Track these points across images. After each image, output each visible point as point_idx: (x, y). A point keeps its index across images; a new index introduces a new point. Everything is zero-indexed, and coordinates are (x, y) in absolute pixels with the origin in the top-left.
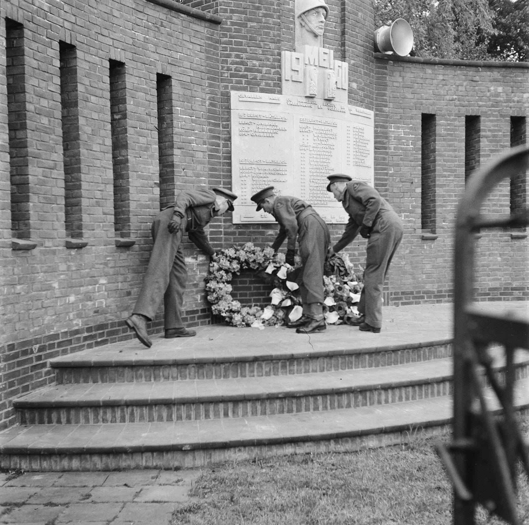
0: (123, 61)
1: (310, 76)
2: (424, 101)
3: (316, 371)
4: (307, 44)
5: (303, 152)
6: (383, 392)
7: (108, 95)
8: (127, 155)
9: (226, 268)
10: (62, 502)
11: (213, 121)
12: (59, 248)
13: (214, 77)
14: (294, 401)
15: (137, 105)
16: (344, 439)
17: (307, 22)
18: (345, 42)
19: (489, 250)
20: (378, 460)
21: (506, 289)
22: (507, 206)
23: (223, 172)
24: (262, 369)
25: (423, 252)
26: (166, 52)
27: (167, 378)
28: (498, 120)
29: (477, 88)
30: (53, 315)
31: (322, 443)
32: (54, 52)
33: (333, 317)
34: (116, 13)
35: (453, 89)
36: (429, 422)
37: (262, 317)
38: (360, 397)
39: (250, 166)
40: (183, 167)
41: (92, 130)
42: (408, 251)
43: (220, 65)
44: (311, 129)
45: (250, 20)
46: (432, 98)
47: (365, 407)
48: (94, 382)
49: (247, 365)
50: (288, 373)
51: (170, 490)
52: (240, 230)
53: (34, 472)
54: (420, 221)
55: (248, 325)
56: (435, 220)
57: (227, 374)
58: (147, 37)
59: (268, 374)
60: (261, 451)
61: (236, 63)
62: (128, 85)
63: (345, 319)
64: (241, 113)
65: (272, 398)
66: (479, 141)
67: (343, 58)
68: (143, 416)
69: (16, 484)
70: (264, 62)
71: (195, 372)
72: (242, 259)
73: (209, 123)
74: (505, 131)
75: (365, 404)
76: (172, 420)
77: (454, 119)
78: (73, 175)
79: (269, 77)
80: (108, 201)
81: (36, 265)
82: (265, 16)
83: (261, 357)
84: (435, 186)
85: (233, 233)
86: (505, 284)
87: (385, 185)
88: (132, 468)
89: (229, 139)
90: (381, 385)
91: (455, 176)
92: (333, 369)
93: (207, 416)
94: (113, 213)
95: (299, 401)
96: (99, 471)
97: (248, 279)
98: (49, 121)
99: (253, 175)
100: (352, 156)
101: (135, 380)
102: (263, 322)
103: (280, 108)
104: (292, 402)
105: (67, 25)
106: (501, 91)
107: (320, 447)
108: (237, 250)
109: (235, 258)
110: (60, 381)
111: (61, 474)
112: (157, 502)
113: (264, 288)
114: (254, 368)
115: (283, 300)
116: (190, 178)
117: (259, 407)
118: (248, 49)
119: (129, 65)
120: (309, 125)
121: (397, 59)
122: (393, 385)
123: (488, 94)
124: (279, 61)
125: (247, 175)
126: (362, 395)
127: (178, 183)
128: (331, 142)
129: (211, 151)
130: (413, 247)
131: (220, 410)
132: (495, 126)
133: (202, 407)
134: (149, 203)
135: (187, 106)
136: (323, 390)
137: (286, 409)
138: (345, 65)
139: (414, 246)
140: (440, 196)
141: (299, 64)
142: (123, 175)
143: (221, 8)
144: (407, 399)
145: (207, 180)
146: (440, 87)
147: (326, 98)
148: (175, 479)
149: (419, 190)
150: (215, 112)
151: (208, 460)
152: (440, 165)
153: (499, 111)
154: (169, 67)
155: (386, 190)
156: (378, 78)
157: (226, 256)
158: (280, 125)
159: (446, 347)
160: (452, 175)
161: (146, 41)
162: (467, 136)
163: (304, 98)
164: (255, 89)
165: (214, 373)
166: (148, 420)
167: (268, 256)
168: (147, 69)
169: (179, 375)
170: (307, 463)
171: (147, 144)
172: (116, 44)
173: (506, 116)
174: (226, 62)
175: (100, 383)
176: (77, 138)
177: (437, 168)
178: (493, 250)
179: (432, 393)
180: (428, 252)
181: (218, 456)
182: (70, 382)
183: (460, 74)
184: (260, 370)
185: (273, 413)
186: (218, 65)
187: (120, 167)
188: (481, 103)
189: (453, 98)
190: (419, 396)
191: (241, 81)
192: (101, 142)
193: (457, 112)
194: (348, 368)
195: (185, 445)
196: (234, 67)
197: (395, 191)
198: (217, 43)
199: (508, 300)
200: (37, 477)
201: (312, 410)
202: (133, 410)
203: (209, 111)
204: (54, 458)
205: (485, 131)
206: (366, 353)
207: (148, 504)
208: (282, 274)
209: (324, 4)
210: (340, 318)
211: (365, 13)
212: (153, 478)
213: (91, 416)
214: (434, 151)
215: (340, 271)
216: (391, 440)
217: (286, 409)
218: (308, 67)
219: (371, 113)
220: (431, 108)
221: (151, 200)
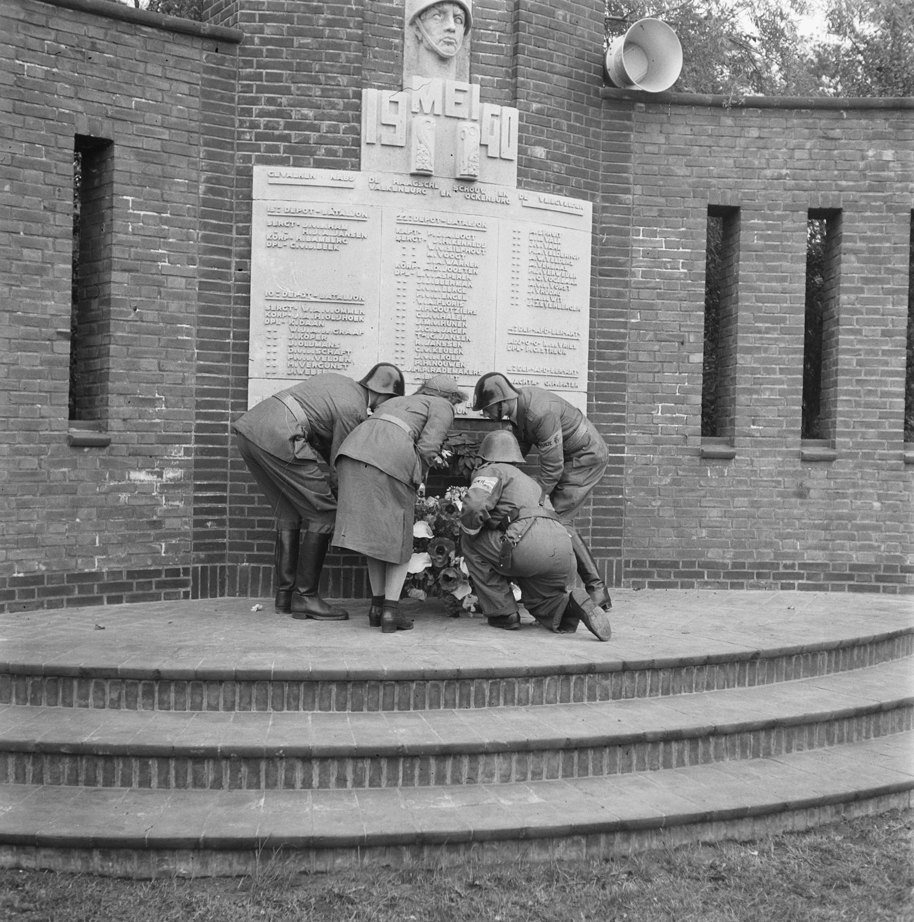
2: (714, 181)
5: (402, 279)
6: (299, 765)
11: (214, 222)
16: (122, 852)
18: (516, 69)
19: (854, 485)
21: (888, 568)
23: (234, 315)
24: (104, 694)
25: (702, 483)
26: (103, 97)
29: (836, 152)
35: (780, 156)
36: (313, 838)
38: (244, 769)
40: (134, 305)
42: (668, 480)
43: (237, 118)
44: (423, 236)
45: (301, 33)
50: (156, 706)
57: (38, 696)
58: (55, 70)
59: (115, 705)
64: (271, 205)
67: (513, 100)
70: (325, 111)
73: (205, 226)
74: (897, 241)
82: (330, 23)
86: (888, 558)
87: (621, 346)
89: (248, 255)
91: (784, 331)
92: (254, 705)
95: (109, 764)
103: (353, 196)
104: (96, 765)
114: (88, 690)
116: (152, 324)
117: (30, 768)
118: (293, 87)
120: (416, 228)
122: (315, 753)
123: (862, 164)
124: (358, 108)
125: (279, 321)
128: (470, 260)
129: (205, 275)
130: (680, 473)
132: (874, 229)
134: (40, 368)
137: (82, 777)
138: (512, 114)
139: (684, 470)
140: (745, 370)
141: (397, 113)
146: (752, 152)
147: (458, 176)
152: (747, 308)
153: (884, 199)
154: (107, 124)
155: (623, 357)
156: (610, 138)
158: (353, 228)
160: (775, 329)
163: (409, 177)
164: (305, 162)
165: (14, 693)
168: (50, 130)
171: (43, 262)
173: (901, 209)
174: (249, 112)
178: (863, 486)
180: (714, 484)
185: (56, 781)
186: (233, 119)
188: (844, 183)
189: (780, 174)
190: (389, 780)
193: (789, 201)
194: (289, 709)
196: (263, 120)
197: (641, 358)
198: (230, 77)
201: (135, 786)
205: (851, 239)
216: (230, 865)
217: (82, 777)
218: (420, 120)
220: (729, 194)
221: (51, 363)
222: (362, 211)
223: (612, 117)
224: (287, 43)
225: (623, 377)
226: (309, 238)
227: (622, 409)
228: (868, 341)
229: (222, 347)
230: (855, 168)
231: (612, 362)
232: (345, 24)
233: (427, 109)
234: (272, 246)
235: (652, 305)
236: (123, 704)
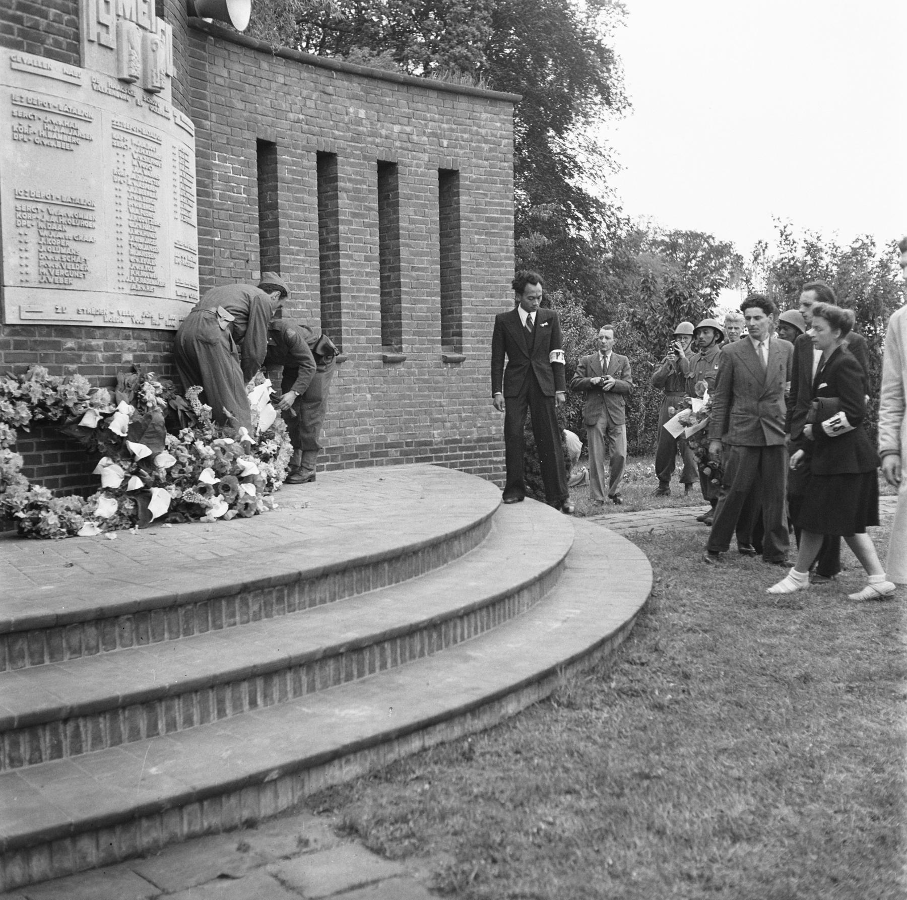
1: (129, 41)
2: (259, 117)
5: (118, 186)
19: (355, 382)
21: (378, 446)
24: (248, 607)
27: (76, 651)
37: (97, 514)
46: (270, 114)
47: (440, 652)
49: (224, 603)
52: (17, 338)
59: (257, 617)
60: (378, 753)
68: (100, 736)
77: (302, 155)
79: (59, 30)
88: (161, 844)
93: (221, 712)
96: (93, 868)
99: (42, 225)
101: (8, 666)
107: (453, 730)
108: (21, 382)
109: (20, 399)
120: (127, 136)
123: (347, 119)
131: (243, 696)
132: (357, 173)
133: (211, 695)
151: (299, 793)
153: (361, 149)
163: (117, 81)
166: (109, 742)
169: (100, 642)
178: (360, 382)
184: (244, 609)
189: (299, 119)
193: (304, 143)
195: (272, 770)
199: (382, 465)
201: (377, 670)
202: (78, 727)
208: (119, 425)
222: (86, 110)
228: (358, 264)
230: (342, 121)
235: (227, 225)
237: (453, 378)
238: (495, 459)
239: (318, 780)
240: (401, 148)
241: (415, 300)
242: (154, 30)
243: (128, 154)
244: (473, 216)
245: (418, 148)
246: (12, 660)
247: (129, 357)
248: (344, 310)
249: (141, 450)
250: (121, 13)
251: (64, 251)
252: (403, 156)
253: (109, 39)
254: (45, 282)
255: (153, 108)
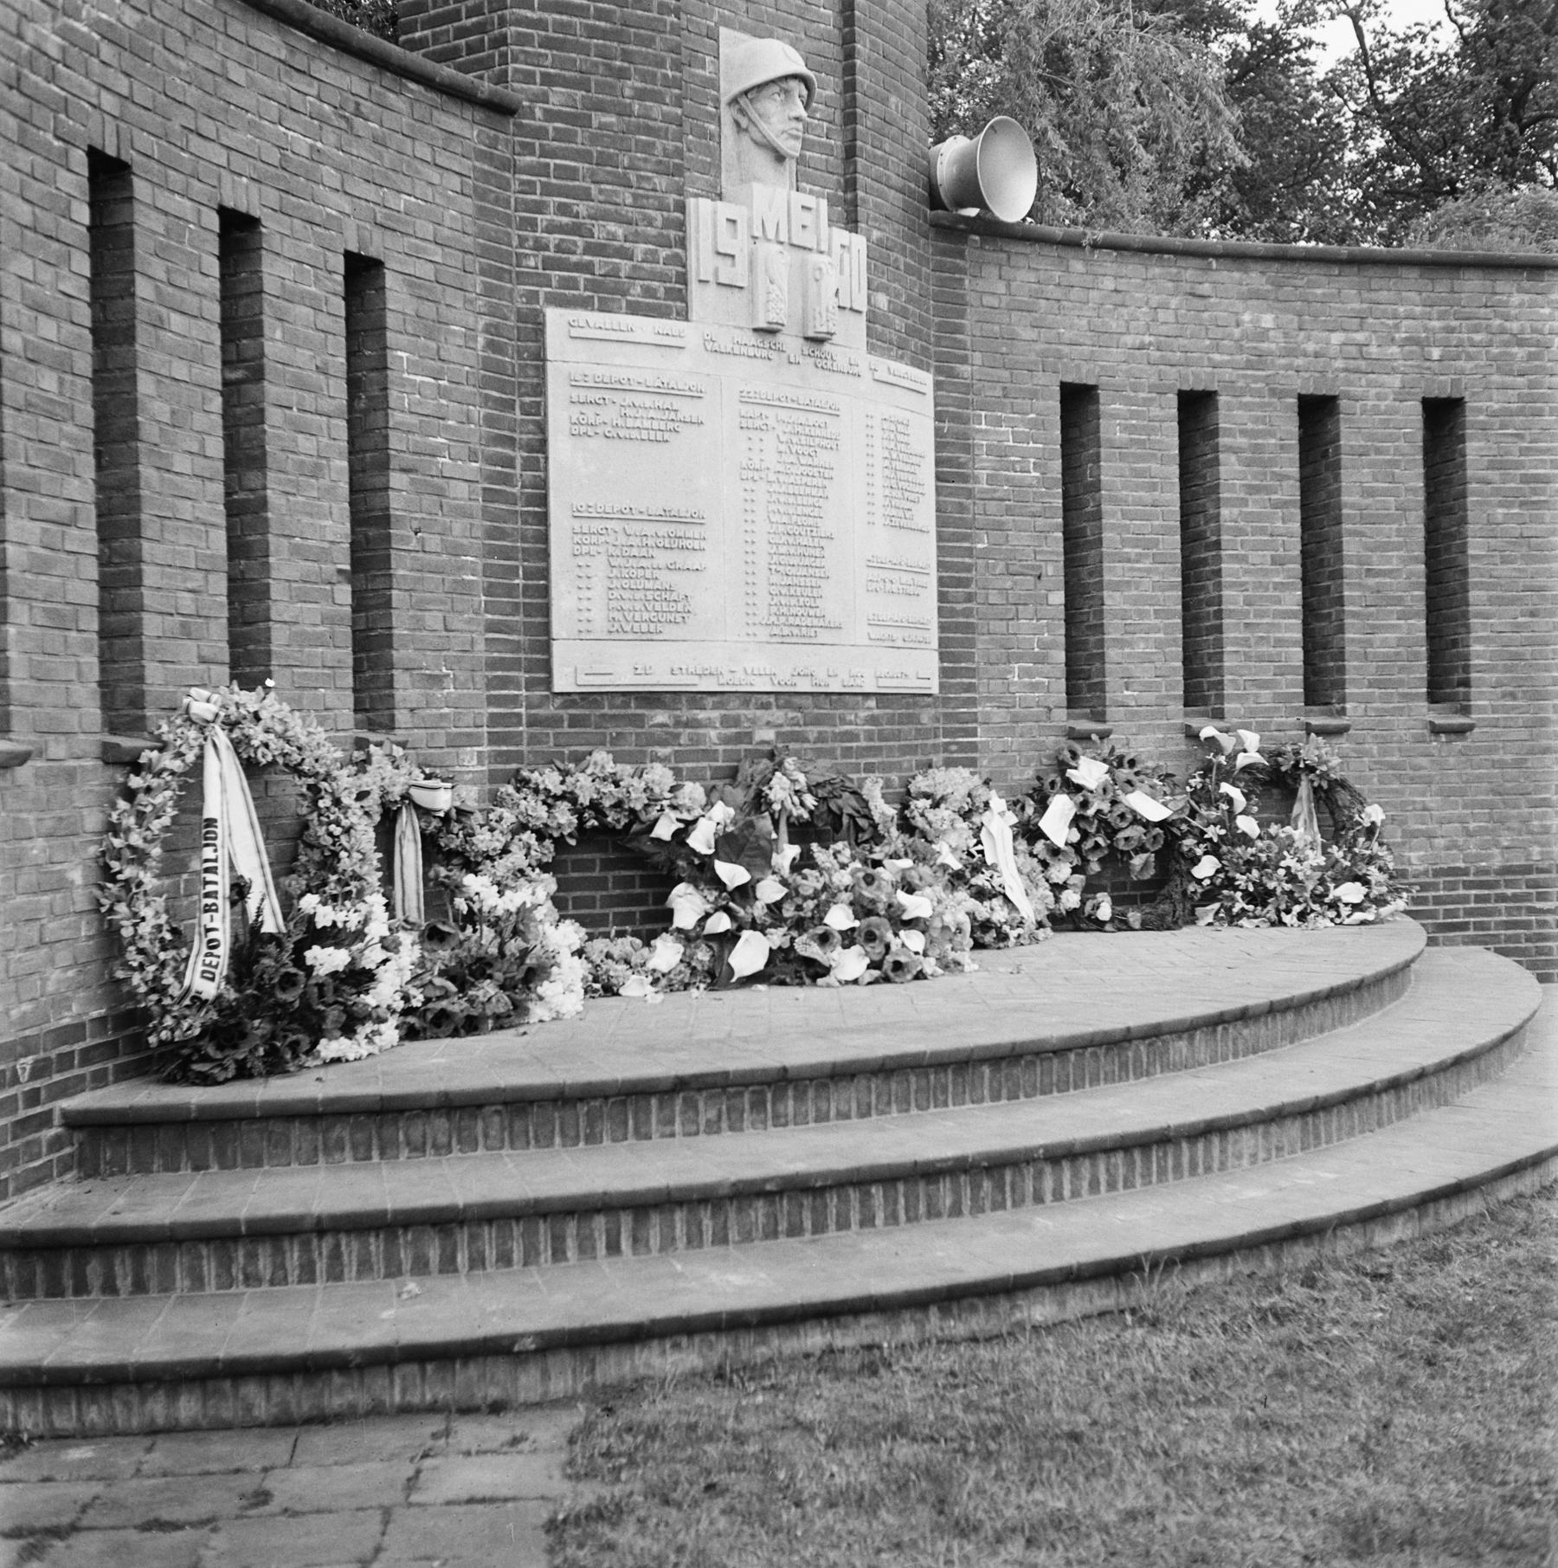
0: (256, 213)
2: (1066, 349)
3: (847, 1116)
4: (757, 179)
5: (749, 485)
7: (214, 310)
8: (265, 488)
9: (539, 824)
10: (194, 1518)
12: (83, 763)
13: (498, 266)
14: (807, 1201)
15: (292, 341)
16: (965, 1303)
17: (754, 116)
20: (1071, 1355)
22: (1294, 644)
23: (524, 540)
27: (418, 1149)
28: (1262, 406)
30: (70, 967)
31: (907, 1315)
32: (74, 181)
33: (850, 963)
34: (237, 74)
37: (650, 966)
38: (987, 1185)
39: (604, 524)
40: (415, 525)
41: (173, 412)
44: (771, 422)
45: (601, 107)
48: (196, 1168)
49: (654, 1102)
51: (508, 1468)
53: (62, 1438)
54: (1062, 684)
55: (610, 990)
56: (1102, 684)
59: (713, 1128)
60: (736, 1345)
61: (561, 229)
62: (270, 285)
63: (887, 966)
65: (745, 1193)
66: (1216, 462)
67: (851, 222)
69: (21, 1475)
71: (503, 1129)
72: (584, 800)
75: (999, 1205)
76: (456, 1270)
78: (116, 544)
80: (212, 623)
81: (24, 815)
82: (640, 95)
83: (696, 1077)
84: (1100, 586)
85: (555, 721)
87: (965, 583)
88: (361, 1411)
89: (542, 446)
90: (1046, 1148)
93: (559, 1254)
94: (227, 659)
96: (262, 1425)
97: (598, 856)
98: (61, 382)
99: (612, 550)
100: (879, 500)
101: (321, 1158)
102: (655, 982)
103: (684, 361)
105: (108, 102)
106: (1270, 325)
108: (565, 773)
109: (562, 797)
110: (88, 1167)
111: (147, 1442)
112: (483, 1501)
113: (645, 882)
115: (707, 915)
117: (707, 1223)
119: (271, 226)
120: (765, 411)
121: (994, 231)
122: (1077, 1148)
123: (1237, 332)
124: (681, 226)
125: (593, 550)
126: (991, 1177)
127: (401, 572)
128: (824, 457)
129: (491, 478)
132: (1256, 420)
135: (427, 348)
136: (889, 1166)
138: (859, 242)
142: (248, 545)
143: (516, 71)
144: (1112, 1186)
145: (480, 562)
147: (811, 334)
148: (505, 1435)
149: (1058, 598)
150: (499, 368)
151: (586, 1379)
152: (1113, 527)
154: (377, 234)
155: (970, 598)
156: (942, 283)
157: (536, 791)
158: (686, 409)
159: (1192, 1038)
161: (316, 156)
162: (1183, 448)
167: (657, 790)
170: (875, 1373)
172: (238, 162)
174: (533, 225)
175: (215, 1169)
176: (132, 433)
177: (1107, 535)
179: (1178, 1167)
181: (614, 1367)
182: (123, 1171)
183: (1161, 277)
184: (691, 1114)
185: (747, 1237)
187: (245, 518)
188: (1217, 357)
191: (575, 280)
192: (195, 449)
193: (1154, 380)
195: (523, 1335)
196: (554, 238)
200: (78, 1453)
201: (855, 1227)
202: (337, 1246)
203: (487, 364)
204: (120, 1392)
205: (1230, 433)
206: (983, 1061)
207: (458, 1509)
208: (701, 841)
209: (800, 67)
210: (874, 965)
211: (906, 99)
212: (434, 1436)
213: (210, 1268)
214: (1096, 487)
215: (859, 829)
218: (762, 247)
219: (926, 379)
220: (1085, 367)
222: (692, 382)
223: (944, 253)
224: (585, 122)
225: (970, 628)
226: (630, 423)
227: (971, 672)
229: (510, 591)
230: (1230, 337)
231: (959, 607)
232: (658, 98)
233: (771, 234)
234: (580, 431)
236: (724, 1125)
237: (1452, 760)
238: (1539, 905)
239: (619, 1364)
240: (1346, 370)
241: (1373, 627)
242: (824, 247)
243: (769, 438)
244: (1493, 475)
245: (1383, 366)
246: (328, 1151)
247: (769, 735)
248: (1228, 649)
249: (732, 874)
250: (758, 233)
251: (649, 585)
252: (1350, 383)
253: (738, 274)
254: (616, 633)
255: (821, 363)
